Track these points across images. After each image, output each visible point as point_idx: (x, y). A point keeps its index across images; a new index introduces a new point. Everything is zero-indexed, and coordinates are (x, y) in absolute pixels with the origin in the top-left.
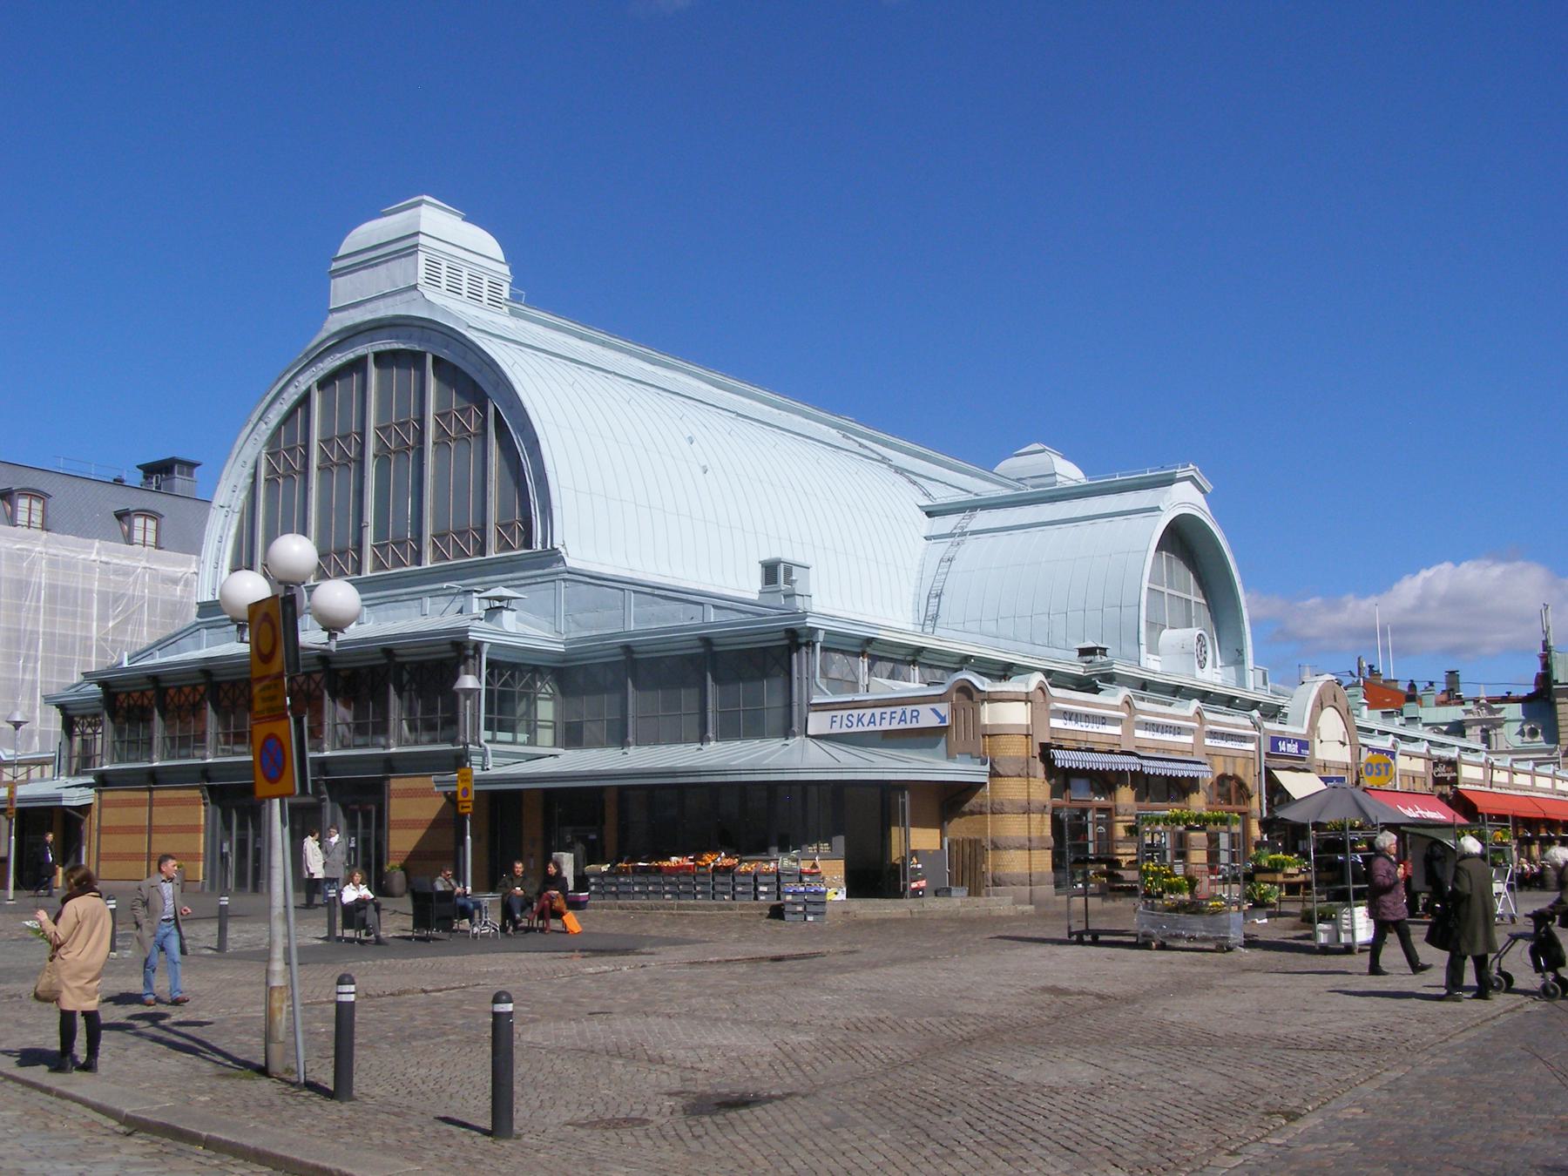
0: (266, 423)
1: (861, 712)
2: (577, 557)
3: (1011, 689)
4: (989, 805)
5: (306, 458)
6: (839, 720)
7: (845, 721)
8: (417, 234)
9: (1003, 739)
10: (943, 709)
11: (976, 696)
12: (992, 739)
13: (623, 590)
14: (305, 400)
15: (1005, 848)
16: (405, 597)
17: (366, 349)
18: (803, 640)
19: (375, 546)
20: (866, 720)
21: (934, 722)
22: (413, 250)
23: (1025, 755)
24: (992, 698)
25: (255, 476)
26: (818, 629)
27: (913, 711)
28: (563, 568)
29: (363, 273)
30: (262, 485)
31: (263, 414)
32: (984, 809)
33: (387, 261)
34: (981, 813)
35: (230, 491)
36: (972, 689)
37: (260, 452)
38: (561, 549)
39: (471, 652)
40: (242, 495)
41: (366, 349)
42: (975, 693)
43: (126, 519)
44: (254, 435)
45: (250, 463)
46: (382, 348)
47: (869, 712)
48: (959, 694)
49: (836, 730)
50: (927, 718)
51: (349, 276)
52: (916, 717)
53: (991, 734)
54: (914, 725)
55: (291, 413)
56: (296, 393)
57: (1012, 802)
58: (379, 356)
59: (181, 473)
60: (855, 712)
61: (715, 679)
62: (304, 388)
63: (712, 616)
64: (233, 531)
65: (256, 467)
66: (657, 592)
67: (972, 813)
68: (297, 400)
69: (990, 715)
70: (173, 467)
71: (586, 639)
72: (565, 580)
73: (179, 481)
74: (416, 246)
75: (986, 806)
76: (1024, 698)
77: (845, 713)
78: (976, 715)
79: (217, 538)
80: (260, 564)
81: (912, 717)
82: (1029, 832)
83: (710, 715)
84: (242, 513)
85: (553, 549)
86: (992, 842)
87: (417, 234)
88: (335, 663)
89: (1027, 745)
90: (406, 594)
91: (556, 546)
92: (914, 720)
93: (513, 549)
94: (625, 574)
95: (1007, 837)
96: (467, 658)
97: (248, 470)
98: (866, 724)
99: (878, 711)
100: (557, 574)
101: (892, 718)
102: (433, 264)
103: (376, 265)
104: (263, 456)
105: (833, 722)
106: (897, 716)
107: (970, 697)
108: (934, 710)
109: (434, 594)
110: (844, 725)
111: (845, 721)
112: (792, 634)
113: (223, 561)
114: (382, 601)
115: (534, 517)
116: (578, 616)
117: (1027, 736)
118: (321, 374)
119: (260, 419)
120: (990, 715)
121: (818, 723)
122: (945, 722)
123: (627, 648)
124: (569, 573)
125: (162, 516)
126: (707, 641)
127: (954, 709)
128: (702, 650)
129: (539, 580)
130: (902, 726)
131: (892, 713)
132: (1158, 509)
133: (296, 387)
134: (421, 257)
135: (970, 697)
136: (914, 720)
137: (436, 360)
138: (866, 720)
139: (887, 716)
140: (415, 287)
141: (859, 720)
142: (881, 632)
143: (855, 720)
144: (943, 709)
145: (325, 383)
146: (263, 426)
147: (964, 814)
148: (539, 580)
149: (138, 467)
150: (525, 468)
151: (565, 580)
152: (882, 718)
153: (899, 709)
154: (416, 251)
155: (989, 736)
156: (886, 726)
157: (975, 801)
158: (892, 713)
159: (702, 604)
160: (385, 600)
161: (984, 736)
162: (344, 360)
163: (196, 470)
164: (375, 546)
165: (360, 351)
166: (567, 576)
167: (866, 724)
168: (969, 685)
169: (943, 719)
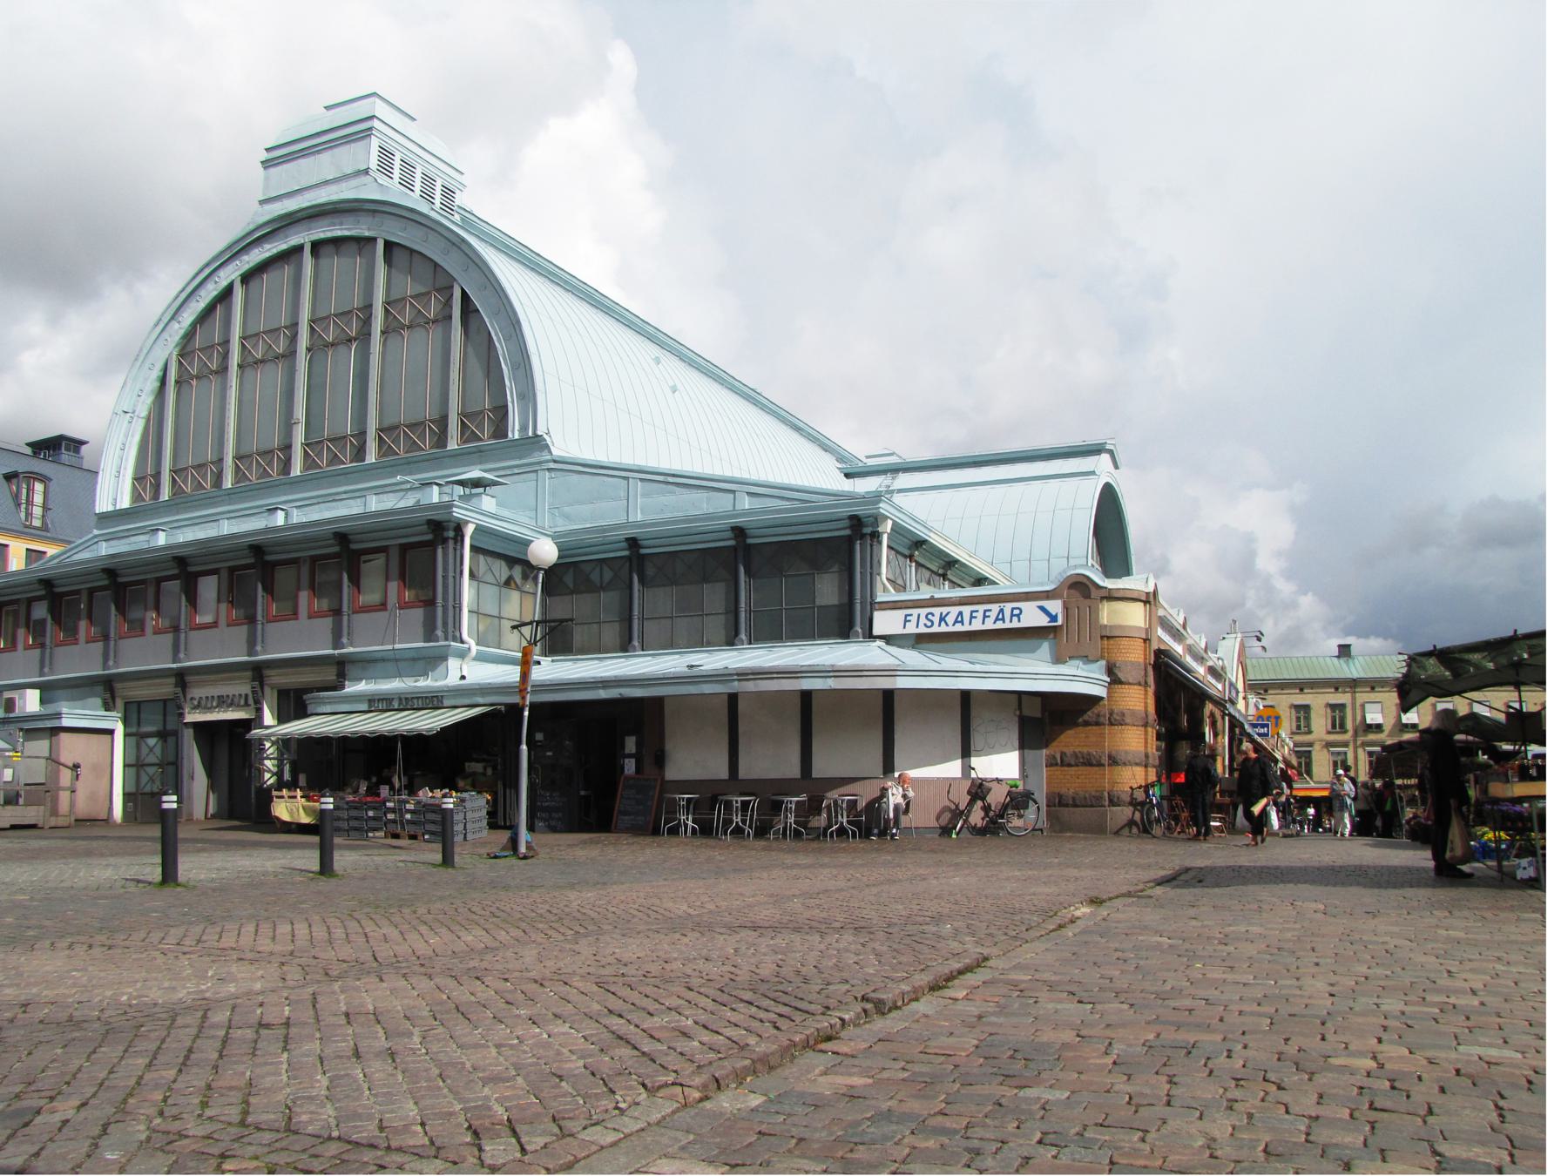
0: (179, 322)
1: (945, 610)
2: (562, 445)
3: (1132, 587)
4: (1107, 716)
5: (225, 356)
6: (914, 619)
7: (923, 620)
8: (372, 117)
9: (1124, 642)
10: (1055, 606)
11: (1094, 593)
12: (1112, 642)
13: (626, 478)
14: (227, 293)
15: (1125, 764)
16: (344, 496)
17: (302, 237)
18: (867, 530)
19: (307, 445)
20: (950, 619)
21: (1043, 621)
22: (367, 134)
23: (1141, 660)
24: (1111, 596)
25: (163, 381)
26: (888, 517)
27: (1013, 609)
28: (549, 457)
29: (302, 161)
30: (172, 388)
31: (176, 313)
32: (1102, 719)
33: (331, 148)
34: (1097, 724)
35: (135, 397)
36: (1090, 585)
37: (171, 353)
38: (545, 436)
39: (451, 534)
40: (148, 399)
41: (302, 237)
42: (1093, 589)
43: (15, 481)
44: (165, 335)
45: (160, 365)
46: (322, 236)
47: (955, 610)
48: (1072, 591)
49: (911, 629)
50: (1032, 616)
51: (285, 166)
52: (1018, 616)
53: (1109, 637)
54: (1015, 624)
55: (209, 310)
56: (215, 289)
57: (1133, 713)
58: (316, 246)
59: (68, 449)
60: (937, 611)
61: (748, 573)
62: (225, 283)
63: (746, 503)
64: (137, 438)
65: (165, 370)
66: (671, 479)
67: (1086, 724)
68: (216, 296)
69: (1109, 614)
70: (60, 445)
71: (586, 531)
72: (549, 470)
73: (65, 456)
74: (370, 129)
75: (1105, 716)
76: (1144, 598)
77: (923, 611)
78: (1094, 613)
79: (119, 445)
80: (168, 470)
81: (1012, 615)
82: (1146, 747)
83: (742, 615)
84: (148, 420)
85: (537, 436)
86: (1110, 757)
87: (372, 117)
88: (271, 554)
89: (1145, 650)
90: (345, 492)
91: (539, 433)
92: (1015, 619)
93: (481, 440)
94: (627, 460)
95: (1126, 752)
96: (445, 541)
97: (157, 373)
98: (950, 623)
99: (966, 610)
100: (540, 463)
101: (985, 617)
102: (386, 154)
103: (319, 152)
104: (174, 357)
105: (906, 621)
106: (993, 615)
107: (1087, 596)
108: (1042, 609)
109: (380, 490)
110: (921, 624)
111: (923, 620)
112: (856, 522)
113: (125, 469)
114: (315, 501)
115: (510, 405)
116: (567, 509)
117: (1145, 640)
118: (247, 267)
119: (172, 318)
120: (1109, 614)
121: (885, 622)
122: (1056, 621)
123: (633, 543)
124: (555, 461)
125: (50, 480)
126: (739, 532)
127: (1066, 608)
128: (732, 543)
129: (516, 471)
130: (999, 625)
131: (985, 611)
132: (1093, 473)
133: (216, 282)
134: (375, 143)
135: (1087, 596)
136: (1015, 619)
137: (389, 245)
138: (950, 619)
139: (980, 615)
140: (366, 172)
141: (942, 619)
142: (932, 535)
143: (936, 620)
144: (1055, 606)
145: (246, 278)
146: (175, 325)
147: (1077, 725)
148: (516, 471)
149: (28, 444)
150: (500, 352)
151: (549, 470)
152: (972, 617)
153: (995, 608)
154: (370, 135)
155: (1108, 637)
156: (977, 625)
157: (1089, 716)
158: (985, 611)
159: (734, 492)
160: (320, 500)
161: (1102, 637)
162: (275, 251)
163: (84, 448)
164: (307, 445)
165: (294, 241)
166: (552, 465)
167: (950, 623)
168: (1085, 581)
169: (1053, 618)
